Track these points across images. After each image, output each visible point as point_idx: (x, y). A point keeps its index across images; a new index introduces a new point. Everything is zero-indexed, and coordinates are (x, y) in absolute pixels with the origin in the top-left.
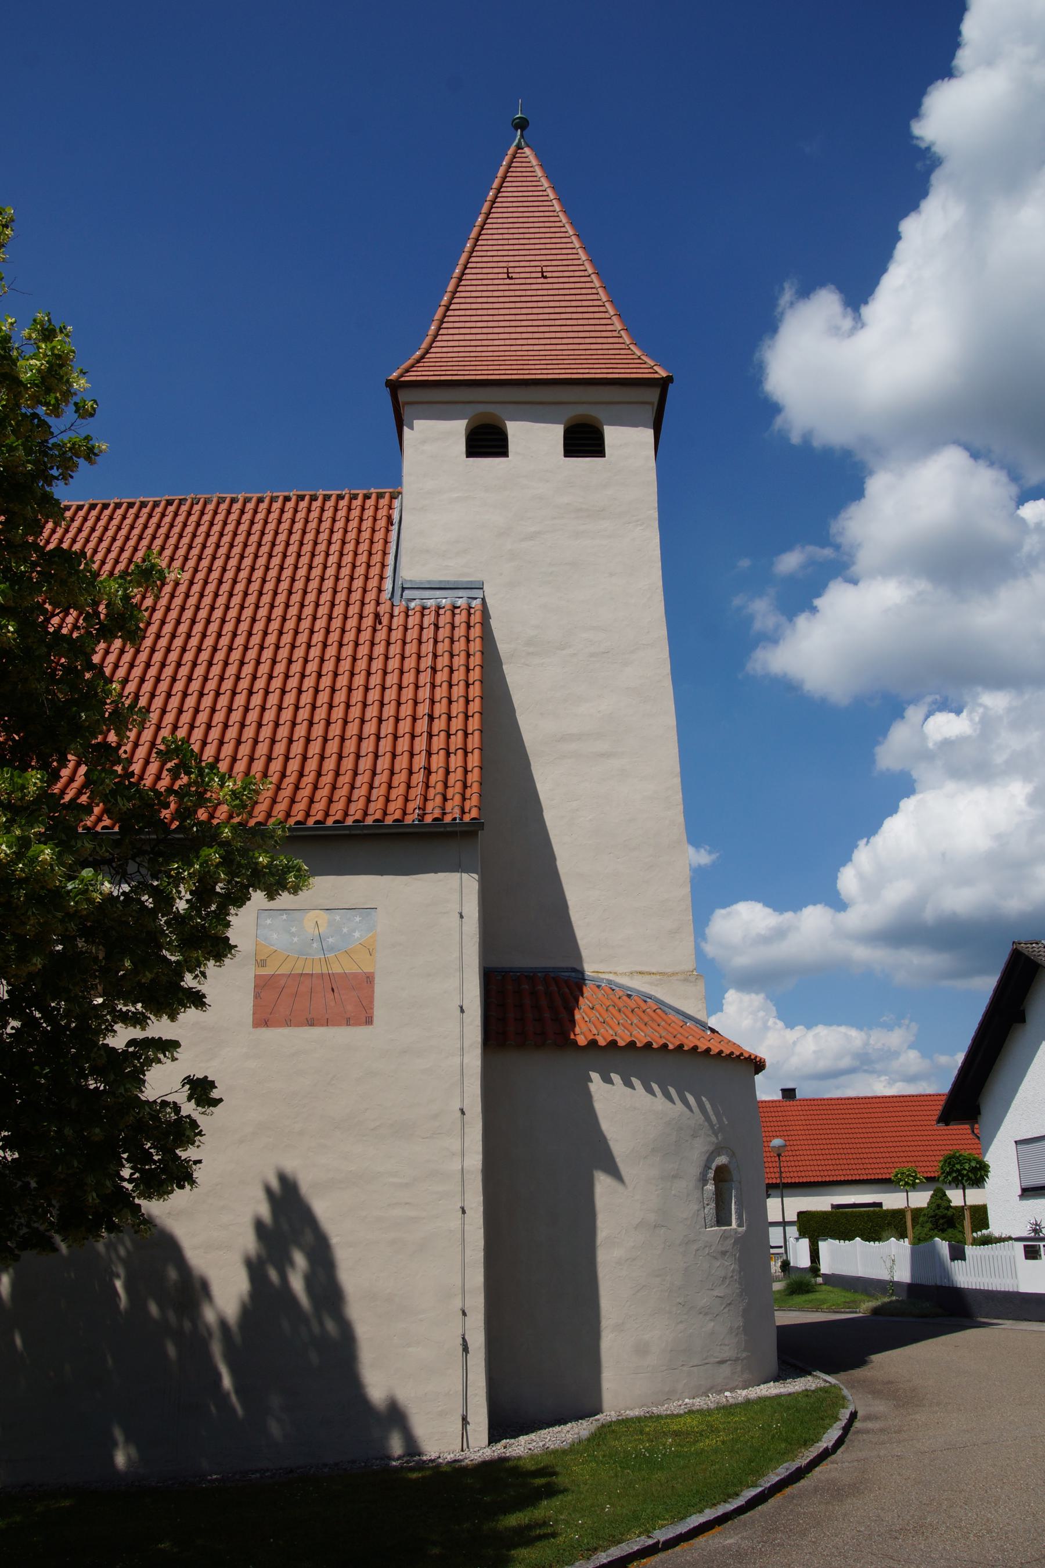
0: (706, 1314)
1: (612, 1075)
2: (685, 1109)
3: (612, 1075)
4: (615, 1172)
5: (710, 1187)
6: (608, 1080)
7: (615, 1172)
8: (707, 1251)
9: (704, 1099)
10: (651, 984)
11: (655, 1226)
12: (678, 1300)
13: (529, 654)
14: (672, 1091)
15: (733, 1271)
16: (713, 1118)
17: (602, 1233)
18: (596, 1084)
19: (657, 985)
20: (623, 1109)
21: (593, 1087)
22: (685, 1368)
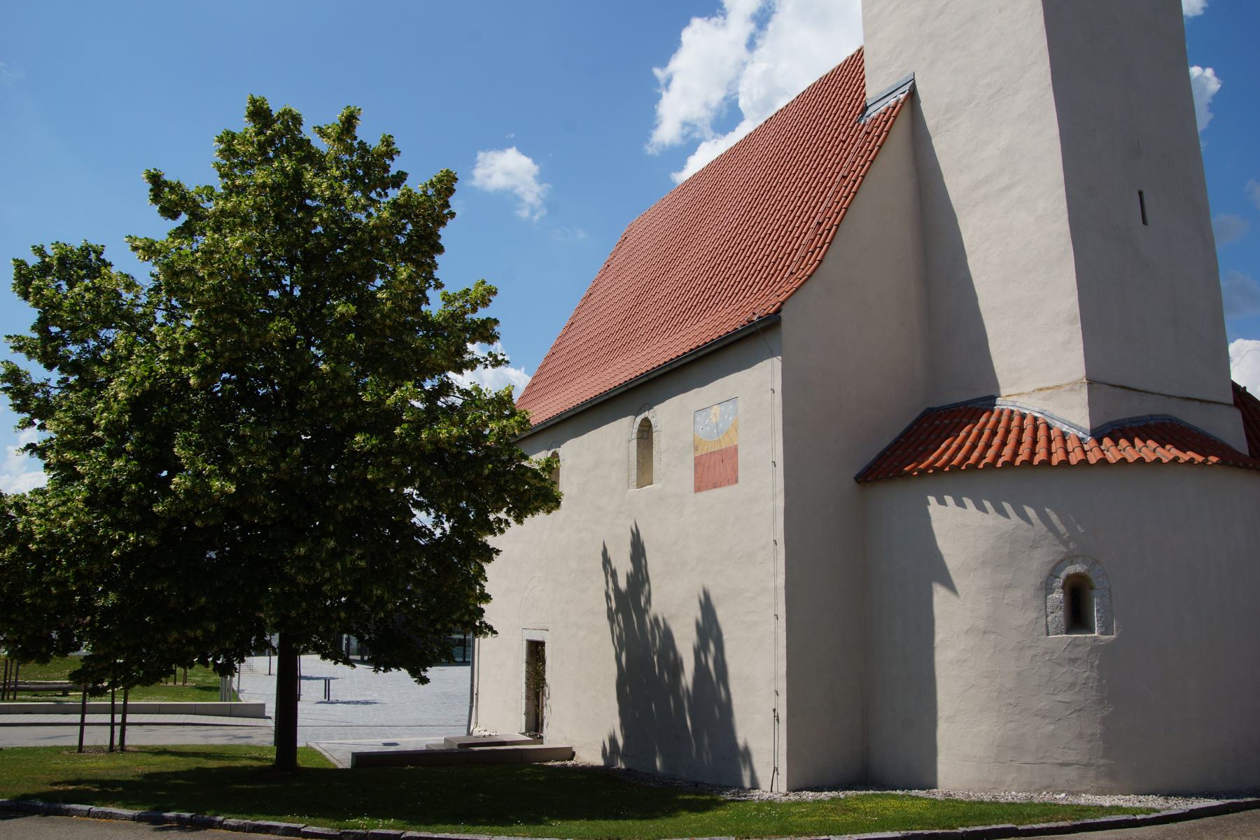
0: (1044, 717)
4: (950, 586)
5: (1058, 596)
6: (942, 502)
7: (950, 586)
9: (1047, 510)
10: (1044, 399)
14: (1007, 506)
15: (1087, 678)
16: (1062, 528)
20: (960, 528)
21: (931, 509)
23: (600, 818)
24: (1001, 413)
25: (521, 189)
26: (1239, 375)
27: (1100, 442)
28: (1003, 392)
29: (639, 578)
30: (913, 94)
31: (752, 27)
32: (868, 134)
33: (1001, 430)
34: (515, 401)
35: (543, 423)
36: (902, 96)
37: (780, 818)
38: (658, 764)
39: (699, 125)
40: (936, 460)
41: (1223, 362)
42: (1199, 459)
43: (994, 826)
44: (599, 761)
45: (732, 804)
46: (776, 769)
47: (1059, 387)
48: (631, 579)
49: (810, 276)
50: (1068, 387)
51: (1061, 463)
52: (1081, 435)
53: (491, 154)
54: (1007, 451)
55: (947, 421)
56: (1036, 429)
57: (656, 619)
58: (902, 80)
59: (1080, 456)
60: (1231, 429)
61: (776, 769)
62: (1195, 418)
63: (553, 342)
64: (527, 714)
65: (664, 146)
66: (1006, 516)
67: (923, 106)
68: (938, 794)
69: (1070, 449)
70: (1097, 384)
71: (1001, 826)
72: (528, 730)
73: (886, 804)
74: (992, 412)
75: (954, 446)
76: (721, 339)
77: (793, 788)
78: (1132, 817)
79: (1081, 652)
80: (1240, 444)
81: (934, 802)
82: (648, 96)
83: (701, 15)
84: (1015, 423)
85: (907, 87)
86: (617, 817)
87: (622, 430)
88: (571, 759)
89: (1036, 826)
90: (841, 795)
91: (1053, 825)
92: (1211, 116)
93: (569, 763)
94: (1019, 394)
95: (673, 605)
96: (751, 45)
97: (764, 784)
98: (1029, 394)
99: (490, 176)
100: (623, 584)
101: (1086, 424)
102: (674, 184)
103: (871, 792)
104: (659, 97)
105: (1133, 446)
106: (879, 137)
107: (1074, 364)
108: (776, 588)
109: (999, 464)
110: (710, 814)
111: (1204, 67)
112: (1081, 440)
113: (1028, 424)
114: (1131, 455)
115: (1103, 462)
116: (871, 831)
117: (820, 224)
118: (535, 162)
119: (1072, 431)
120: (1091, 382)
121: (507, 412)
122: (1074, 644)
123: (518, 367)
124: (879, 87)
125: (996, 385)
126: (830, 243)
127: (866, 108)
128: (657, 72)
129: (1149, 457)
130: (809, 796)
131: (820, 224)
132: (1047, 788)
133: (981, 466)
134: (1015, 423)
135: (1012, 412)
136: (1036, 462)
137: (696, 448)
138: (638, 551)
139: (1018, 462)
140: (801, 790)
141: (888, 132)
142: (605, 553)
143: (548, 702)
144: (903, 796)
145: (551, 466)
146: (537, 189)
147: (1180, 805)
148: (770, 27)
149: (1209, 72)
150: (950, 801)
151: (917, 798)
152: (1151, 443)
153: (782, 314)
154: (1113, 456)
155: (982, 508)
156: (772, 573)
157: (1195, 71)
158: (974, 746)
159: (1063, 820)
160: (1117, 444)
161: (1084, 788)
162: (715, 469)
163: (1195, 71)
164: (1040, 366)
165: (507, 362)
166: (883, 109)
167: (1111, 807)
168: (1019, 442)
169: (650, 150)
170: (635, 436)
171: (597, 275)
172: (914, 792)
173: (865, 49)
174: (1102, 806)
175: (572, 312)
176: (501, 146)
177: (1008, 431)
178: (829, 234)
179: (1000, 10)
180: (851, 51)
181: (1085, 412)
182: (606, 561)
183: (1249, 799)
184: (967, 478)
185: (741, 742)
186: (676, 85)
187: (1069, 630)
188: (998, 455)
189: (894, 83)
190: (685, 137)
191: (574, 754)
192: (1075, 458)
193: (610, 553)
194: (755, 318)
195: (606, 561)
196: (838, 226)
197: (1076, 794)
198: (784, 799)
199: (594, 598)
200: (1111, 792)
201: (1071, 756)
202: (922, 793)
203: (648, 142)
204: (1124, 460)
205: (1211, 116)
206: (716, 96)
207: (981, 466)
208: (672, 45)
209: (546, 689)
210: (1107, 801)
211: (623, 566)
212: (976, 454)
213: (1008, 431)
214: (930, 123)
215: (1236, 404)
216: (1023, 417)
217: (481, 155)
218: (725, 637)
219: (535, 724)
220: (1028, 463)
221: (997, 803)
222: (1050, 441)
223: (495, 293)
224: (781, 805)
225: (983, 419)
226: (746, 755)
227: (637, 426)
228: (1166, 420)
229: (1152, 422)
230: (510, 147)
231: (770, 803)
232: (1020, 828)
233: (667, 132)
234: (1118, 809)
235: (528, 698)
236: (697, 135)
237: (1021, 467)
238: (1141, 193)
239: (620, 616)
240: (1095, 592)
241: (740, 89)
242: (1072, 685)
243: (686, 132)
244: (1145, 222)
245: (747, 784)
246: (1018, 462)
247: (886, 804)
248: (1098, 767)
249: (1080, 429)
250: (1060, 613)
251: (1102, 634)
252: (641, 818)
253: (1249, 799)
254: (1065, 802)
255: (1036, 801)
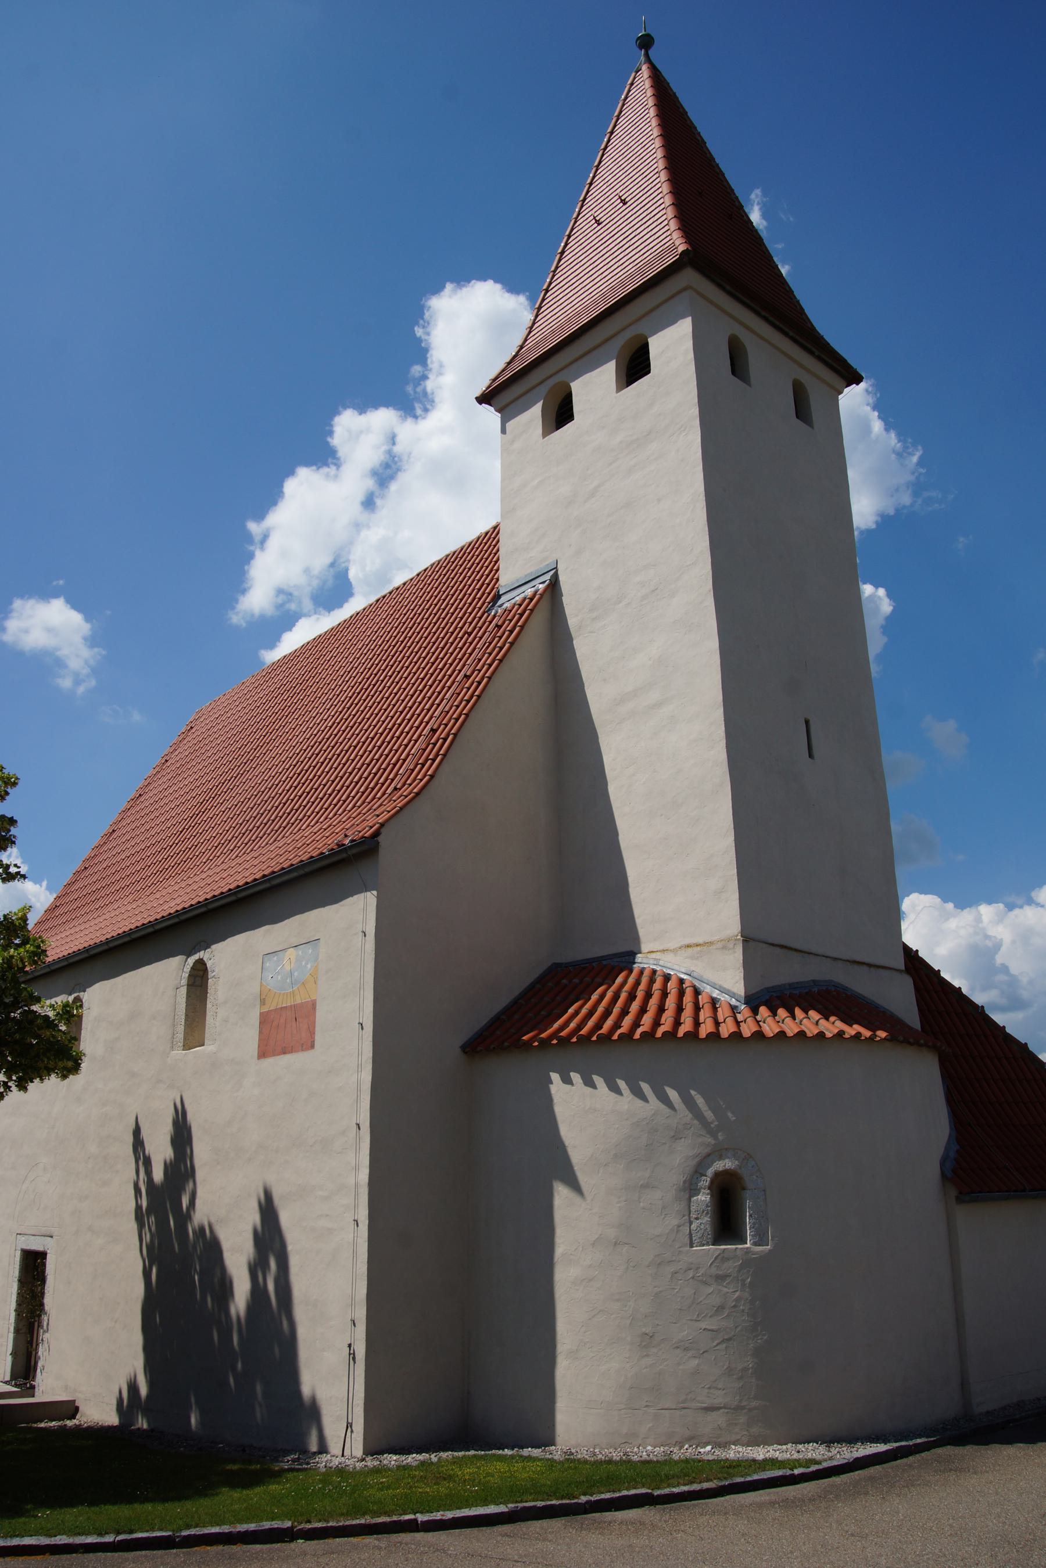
0: (686, 1349)
1: (572, 1074)
2: (662, 1106)
3: (572, 1074)
4: (574, 1185)
5: (704, 1197)
6: (567, 1080)
7: (574, 1185)
8: (691, 1274)
9: (693, 1092)
10: (692, 958)
11: (616, 1243)
12: (644, 1330)
13: (594, 619)
14: (645, 1087)
15: (737, 1300)
16: (709, 1115)
17: (560, 1249)
18: (556, 1086)
19: (697, 959)
20: (587, 1111)
22: (651, 1410)
23: (106, 1501)
24: (641, 972)
25: (64, 652)
26: (912, 935)
27: (755, 1011)
28: (645, 948)
29: (182, 1169)
30: (554, 585)
31: (370, 483)
32: (499, 627)
33: (640, 994)
34: (30, 927)
35: (65, 958)
36: (541, 586)
37: (353, 1492)
38: (193, 1420)
39: (296, 593)
40: (562, 1028)
41: (895, 916)
42: (867, 1033)
43: (625, 1493)
44: (112, 1419)
45: (290, 1475)
46: (349, 1425)
47: (711, 943)
48: (170, 1169)
49: (418, 794)
50: (720, 945)
51: (710, 1035)
52: (733, 1002)
53: (32, 602)
54: (647, 1020)
55: (576, 981)
56: (681, 993)
57: (202, 1229)
58: (543, 566)
59: (732, 1028)
60: (901, 999)
61: (349, 1425)
62: (863, 985)
63: (86, 853)
64: (14, 1354)
65: (253, 615)
66: (645, 1099)
67: (565, 600)
68: (556, 1453)
69: (721, 1019)
70: (752, 941)
71: (633, 1492)
72: (14, 1376)
73: (491, 1469)
74: (631, 971)
75: (584, 1011)
76: (302, 865)
77: (372, 1449)
78: (789, 1472)
79: (730, 1267)
80: (911, 1017)
81: (551, 1463)
82: (237, 556)
83: (308, 463)
84: (657, 985)
85: (548, 577)
86: (129, 1499)
87: (163, 978)
88: (73, 1417)
89: (676, 1490)
90: (434, 1457)
91: (695, 1487)
92: (885, 639)
93: (69, 1423)
94: (663, 951)
95: (223, 1207)
96: (369, 503)
97: (335, 1448)
98: (674, 951)
99: (26, 631)
100: (158, 1175)
101: (740, 989)
102: (264, 663)
103: (472, 1452)
104: (251, 556)
105: (794, 1017)
106: (511, 632)
107: (725, 917)
108: (356, 1185)
109: (637, 1036)
110: (258, 1490)
111: (876, 587)
112: (733, 1009)
113: (672, 986)
114: (791, 1028)
115: (759, 1035)
116: (469, 1506)
117: (434, 731)
118: (88, 619)
119: (724, 998)
120: (747, 940)
121: (17, 941)
122: (722, 1258)
123: (37, 881)
124: (515, 572)
125: (637, 940)
126: (444, 755)
127: (498, 597)
128: (253, 527)
129: (811, 1030)
130: (392, 1460)
131: (434, 731)
132: (690, 1439)
133: (615, 1037)
134: (657, 985)
135: (654, 972)
136: (680, 1034)
137: (263, 1002)
138: (182, 1135)
139: (659, 1034)
140: (382, 1453)
141: (522, 627)
142: (137, 1132)
143: (46, 1336)
144: (512, 1457)
145: (71, 1015)
146: (86, 653)
147: (843, 1454)
148: (393, 487)
149: (881, 592)
150: (571, 1462)
151: (529, 1458)
152: (814, 1014)
153: (380, 839)
154: (770, 1028)
155: (615, 1089)
156: (352, 1167)
157: (867, 589)
158: (597, 1391)
159: (708, 1480)
160: (774, 1014)
161: (734, 1437)
162: (285, 1029)
163: (867, 589)
164: (687, 914)
165: (24, 877)
166: (518, 599)
167: (765, 1460)
168: (661, 1009)
169: (235, 619)
170: (184, 982)
171: (151, 772)
172: (526, 1452)
173: (501, 527)
174: (754, 1460)
175: (114, 816)
176: (46, 594)
177: (648, 995)
178: (447, 744)
179: (659, 500)
180: (483, 526)
181: (739, 975)
182: (138, 1143)
183: (919, 1441)
184: (601, 1053)
185: (306, 1390)
186: (273, 543)
187: (716, 1241)
188: (636, 1024)
189: (532, 569)
190: (279, 607)
191: (77, 1409)
192: (725, 1031)
193: (145, 1134)
194: (347, 842)
195: (138, 1143)
196: (455, 735)
197: (725, 1445)
198: (359, 1465)
199: (119, 1194)
200: (765, 1442)
201: (719, 1398)
202: (536, 1452)
203: (233, 608)
204: (782, 1033)
205: (885, 639)
206: (321, 562)
207: (615, 1037)
208: (269, 496)
209: (45, 1318)
210: (760, 1453)
211: (161, 1151)
212: (609, 1023)
213: (648, 995)
214: (572, 622)
215: (908, 970)
216: (667, 978)
217: (17, 604)
218: (290, 1248)
219: (25, 1368)
220: (671, 1035)
221: (629, 1461)
222: (697, 1008)
223: (14, 784)
224: (354, 1474)
225: (619, 980)
226: (312, 1412)
227: (188, 969)
228: (839, 983)
229: (816, 989)
230: (56, 596)
231: (341, 1471)
232: (656, 1493)
233: (258, 598)
234: (772, 1463)
235: (17, 1331)
236: (293, 606)
237: (664, 1042)
238: (807, 722)
239: (153, 1219)
240: (747, 1194)
241: (352, 557)
242: (720, 1308)
243: (280, 600)
244: (811, 756)
245: (314, 1447)
246: (659, 1034)
247: (491, 1469)
248: (750, 1410)
249: (733, 995)
250: (706, 1219)
251: (755, 1244)
252: (164, 1500)
253: (919, 1441)
254: (710, 1457)
255: (675, 1457)
